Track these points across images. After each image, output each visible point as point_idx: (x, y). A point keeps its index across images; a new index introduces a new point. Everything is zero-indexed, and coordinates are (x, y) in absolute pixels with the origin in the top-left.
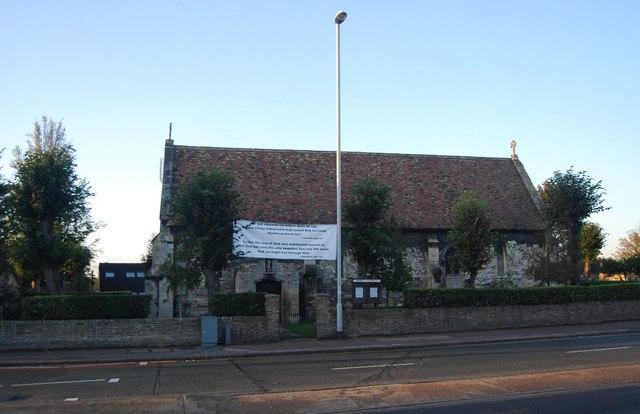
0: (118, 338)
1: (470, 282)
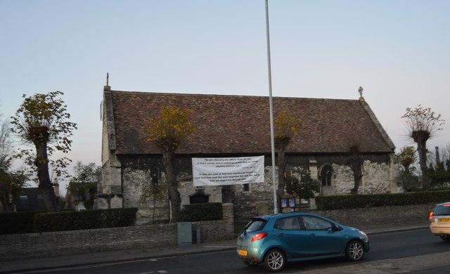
0: (113, 243)
1: (355, 190)
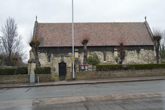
0: (5, 81)
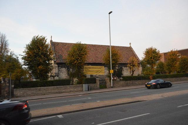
1: (132, 75)
